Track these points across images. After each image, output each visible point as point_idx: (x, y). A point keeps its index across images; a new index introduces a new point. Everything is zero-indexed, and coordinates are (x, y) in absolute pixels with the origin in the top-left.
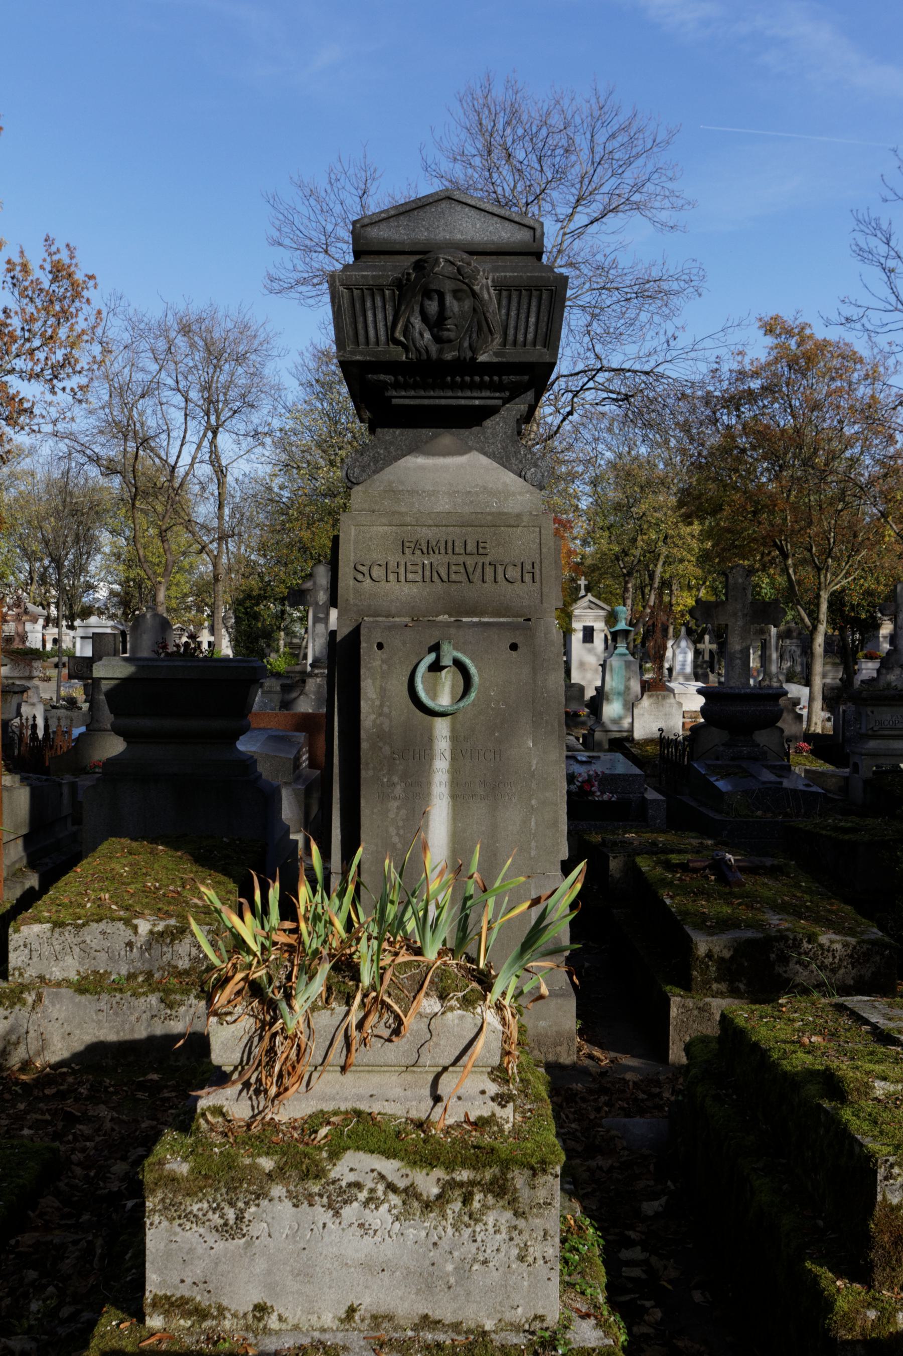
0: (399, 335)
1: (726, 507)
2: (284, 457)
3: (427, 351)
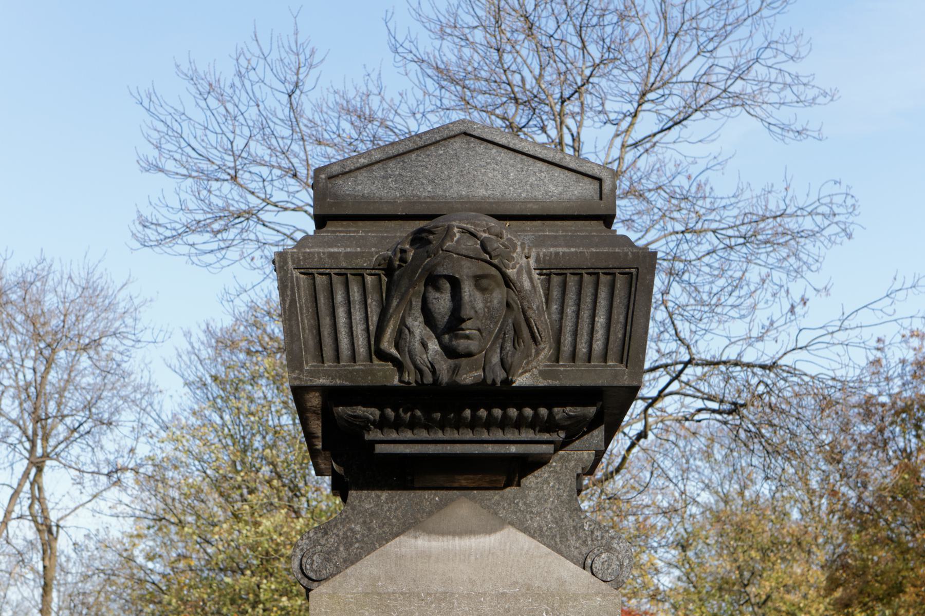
0: (387, 345)
1: (909, 589)
2: (155, 505)
3: (433, 371)
